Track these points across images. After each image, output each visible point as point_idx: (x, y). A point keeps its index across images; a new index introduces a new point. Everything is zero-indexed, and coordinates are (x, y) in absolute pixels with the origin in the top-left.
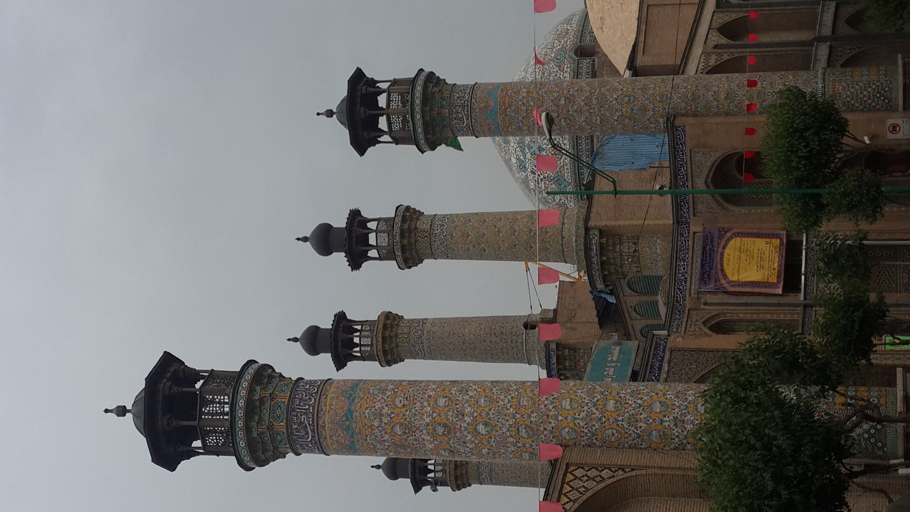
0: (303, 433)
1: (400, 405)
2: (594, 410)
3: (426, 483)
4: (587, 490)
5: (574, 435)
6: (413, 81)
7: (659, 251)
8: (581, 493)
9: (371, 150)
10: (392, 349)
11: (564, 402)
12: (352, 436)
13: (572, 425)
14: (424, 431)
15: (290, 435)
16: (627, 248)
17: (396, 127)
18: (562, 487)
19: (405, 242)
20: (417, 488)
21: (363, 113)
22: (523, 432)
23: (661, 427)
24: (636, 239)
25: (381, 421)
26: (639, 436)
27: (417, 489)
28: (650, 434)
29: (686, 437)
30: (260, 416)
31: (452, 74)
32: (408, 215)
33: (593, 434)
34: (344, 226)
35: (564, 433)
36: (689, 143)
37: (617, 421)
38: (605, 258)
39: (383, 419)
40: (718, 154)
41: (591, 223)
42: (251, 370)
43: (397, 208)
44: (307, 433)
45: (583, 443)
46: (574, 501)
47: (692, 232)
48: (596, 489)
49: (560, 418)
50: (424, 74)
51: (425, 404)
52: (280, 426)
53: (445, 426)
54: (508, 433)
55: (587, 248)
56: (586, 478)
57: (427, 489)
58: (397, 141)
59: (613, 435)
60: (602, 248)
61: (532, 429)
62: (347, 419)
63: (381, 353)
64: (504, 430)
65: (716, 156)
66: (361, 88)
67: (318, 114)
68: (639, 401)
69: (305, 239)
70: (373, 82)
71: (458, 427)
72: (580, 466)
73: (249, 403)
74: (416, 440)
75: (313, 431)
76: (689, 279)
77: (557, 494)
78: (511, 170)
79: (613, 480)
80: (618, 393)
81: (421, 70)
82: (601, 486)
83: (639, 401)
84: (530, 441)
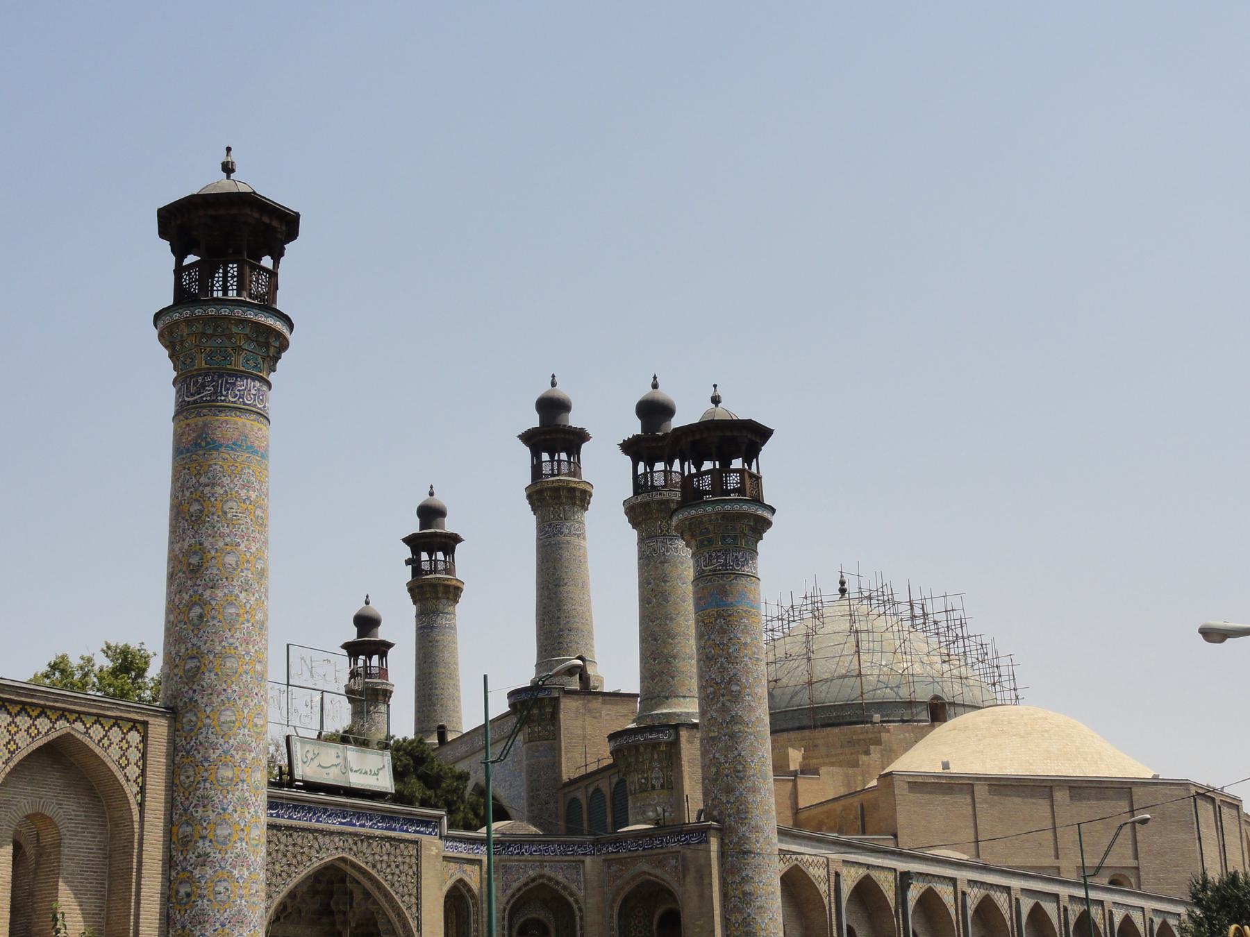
0: (192, 390)
1: (226, 508)
2: (218, 752)
3: (416, 551)
4: (106, 749)
5: (187, 728)
6: (758, 500)
8: (100, 741)
12: (188, 451)
14: (193, 541)
20: (409, 540)
22: (191, 664)
23: (196, 837)
26: (186, 810)
28: (188, 824)
29: (184, 869)
30: (212, 335)
31: (767, 545)
33: (188, 753)
34: (639, 432)
35: (190, 716)
37: (205, 781)
38: (642, 749)
39: (208, 488)
42: (279, 326)
44: (192, 395)
47: (582, 858)
50: (766, 514)
53: (200, 566)
55: (651, 729)
60: (655, 745)
61: (195, 676)
64: (194, 641)
65: (675, 887)
67: (715, 386)
68: (231, 808)
71: (198, 582)
72: (144, 739)
75: (195, 402)
76: (522, 858)
77: (95, 711)
79: (123, 781)
80: (243, 781)
81: (773, 511)
82: (114, 768)
83: (231, 808)
84: (181, 673)
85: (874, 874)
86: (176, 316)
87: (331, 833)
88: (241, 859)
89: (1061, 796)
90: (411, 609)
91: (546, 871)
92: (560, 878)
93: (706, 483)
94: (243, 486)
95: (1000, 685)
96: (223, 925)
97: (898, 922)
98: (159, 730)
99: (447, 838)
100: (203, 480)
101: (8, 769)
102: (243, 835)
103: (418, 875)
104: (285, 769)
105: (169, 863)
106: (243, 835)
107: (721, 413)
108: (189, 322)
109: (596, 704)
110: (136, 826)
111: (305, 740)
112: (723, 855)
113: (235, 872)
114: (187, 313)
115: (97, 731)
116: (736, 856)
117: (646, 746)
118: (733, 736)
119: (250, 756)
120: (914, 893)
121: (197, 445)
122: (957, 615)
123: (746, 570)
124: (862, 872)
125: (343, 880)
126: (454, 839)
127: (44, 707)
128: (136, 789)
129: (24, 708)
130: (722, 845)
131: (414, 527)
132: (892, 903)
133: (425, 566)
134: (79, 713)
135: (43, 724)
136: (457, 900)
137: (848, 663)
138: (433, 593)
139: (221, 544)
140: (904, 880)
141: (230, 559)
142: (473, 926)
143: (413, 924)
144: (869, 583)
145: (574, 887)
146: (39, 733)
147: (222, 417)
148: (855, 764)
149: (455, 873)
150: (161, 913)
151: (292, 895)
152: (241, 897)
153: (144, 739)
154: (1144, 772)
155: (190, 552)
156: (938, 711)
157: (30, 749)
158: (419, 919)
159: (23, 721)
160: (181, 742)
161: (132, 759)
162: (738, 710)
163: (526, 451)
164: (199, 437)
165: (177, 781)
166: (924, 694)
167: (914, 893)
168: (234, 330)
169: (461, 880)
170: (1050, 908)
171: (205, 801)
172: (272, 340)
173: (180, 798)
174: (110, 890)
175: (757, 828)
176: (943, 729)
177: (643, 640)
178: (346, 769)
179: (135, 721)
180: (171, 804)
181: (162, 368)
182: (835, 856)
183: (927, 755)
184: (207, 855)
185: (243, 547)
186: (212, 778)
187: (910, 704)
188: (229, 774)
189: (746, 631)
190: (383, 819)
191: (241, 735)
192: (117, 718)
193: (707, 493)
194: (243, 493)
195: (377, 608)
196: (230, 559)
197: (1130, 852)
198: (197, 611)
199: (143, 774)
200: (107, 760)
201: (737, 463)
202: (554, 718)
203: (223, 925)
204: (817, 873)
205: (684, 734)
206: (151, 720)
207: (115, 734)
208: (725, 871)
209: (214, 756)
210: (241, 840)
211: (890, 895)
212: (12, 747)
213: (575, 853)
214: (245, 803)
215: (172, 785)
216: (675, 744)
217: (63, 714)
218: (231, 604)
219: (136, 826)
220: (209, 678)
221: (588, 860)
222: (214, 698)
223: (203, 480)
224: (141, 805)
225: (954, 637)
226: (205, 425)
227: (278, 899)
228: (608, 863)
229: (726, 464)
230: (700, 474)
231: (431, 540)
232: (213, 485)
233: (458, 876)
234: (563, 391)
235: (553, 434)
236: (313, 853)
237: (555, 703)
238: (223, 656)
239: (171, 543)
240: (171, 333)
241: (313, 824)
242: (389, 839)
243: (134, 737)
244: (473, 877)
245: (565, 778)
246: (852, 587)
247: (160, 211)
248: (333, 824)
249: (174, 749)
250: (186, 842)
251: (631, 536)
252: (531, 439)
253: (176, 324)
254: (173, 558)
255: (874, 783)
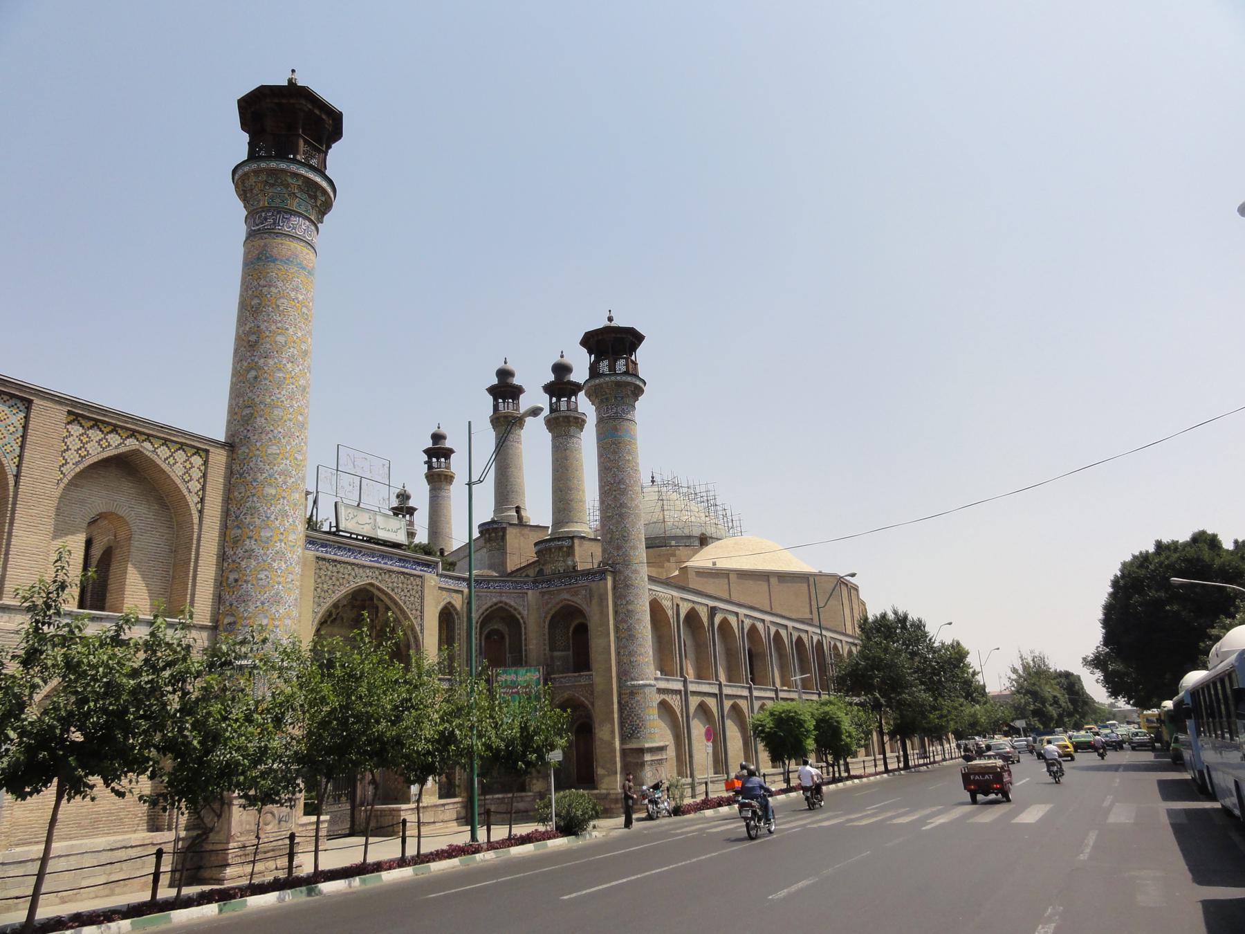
3: (430, 457)
6: (636, 376)
20: (427, 452)
22: (247, 411)
28: (238, 527)
31: (641, 403)
35: (244, 449)
36: (593, 585)
40: (585, 607)
50: (641, 384)
53: (256, 342)
55: (559, 539)
56: (188, 466)
60: (560, 548)
65: (584, 607)
72: (206, 463)
79: (185, 492)
82: (178, 481)
85: (697, 607)
86: (246, 169)
87: (364, 567)
88: (280, 555)
89: (773, 580)
90: (427, 487)
91: (504, 599)
92: (512, 603)
94: (293, 290)
95: (732, 528)
96: (263, 603)
97: (709, 635)
98: (219, 458)
99: (442, 576)
100: (262, 282)
101: (78, 470)
102: (281, 537)
103: (422, 597)
104: (334, 524)
105: (222, 557)
106: (281, 537)
107: (613, 324)
108: (257, 172)
109: (526, 531)
110: (196, 527)
111: (348, 506)
112: (615, 588)
113: (275, 565)
114: (254, 166)
115: (163, 452)
116: (623, 590)
117: (556, 545)
118: (621, 515)
119: (290, 481)
120: (717, 620)
121: (259, 259)
122: (712, 493)
123: (629, 417)
124: (690, 605)
125: (372, 599)
126: (446, 576)
127: (115, 426)
128: (196, 499)
129: (96, 424)
130: (614, 581)
131: (429, 444)
132: (706, 624)
133: (435, 465)
134: (149, 435)
135: (114, 439)
136: (447, 616)
137: (657, 516)
138: (438, 479)
139: (274, 327)
140: (713, 611)
141: (280, 339)
142: (457, 631)
143: (418, 629)
144: (667, 476)
145: (521, 609)
146: (109, 445)
147: (279, 240)
148: (662, 567)
149: (446, 598)
150: (214, 595)
151: (335, 606)
152: (279, 583)
153: (206, 463)
154: (814, 570)
155: (251, 332)
156: (704, 541)
157: (101, 457)
158: (422, 626)
159: (95, 435)
160: (236, 467)
161: (200, 486)
162: (624, 499)
163: (491, 398)
164: (261, 253)
166: (696, 532)
167: (717, 620)
168: (290, 180)
169: (449, 603)
170: (783, 633)
171: (253, 511)
172: (319, 194)
173: (233, 508)
174: (174, 577)
175: (636, 571)
176: (706, 549)
177: (554, 492)
178: (375, 527)
179: (198, 449)
180: (226, 513)
181: (238, 210)
182: (675, 594)
183: (702, 559)
184: (253, 550)
185: (291, 331)
186: (259, 494)
187: (689, 537)
188: (273, 492)
189: (629, 453)
190: (400, 560)
191: (284, 464)
192: (182, 444)
194: (293, 294)
195: (409, 490)
196: (280, 339)
197: (808, 610)
198: (253, 373)
199: (203, 488)
200: (171, 474)
202: (503, 538)
203: (263, 603)
204: (666, 604)
205: (576, 541)
206: (211, 449)
207: (180, 456)
208: (617, 597)
209: (261, 478)
210: (281, 541)
211: (705, 620)
212: (83, 453)
213: (522, 588)
214: (285, 514)
215: (227, 499)
216: (571, 547)
217: (133, 434)
218: (280, 370)
219: (196, 527)
220: (260, 421)
221: (530, 592)
222: (263, 436)
223: (262, 282)
224: (201, 512)
225: (710, 504)
226: (265, 245)
227: (325, 607)
228: (543, 594)
231: (438, 451)
232: (270, 286)
233: (448, 600)
234: (510, 366)
235: (505, 389)
236: (351, 578)
237: (504, 530)
238: (273, 406)
239: (238, 329)
240: (243, 183)
241: (352, 560)
242: (403, 573)
243: (197, 460)
244: (458, 601)
245: (509, 571)
246: (658, 479)
247: (239, 101)
248: (365, 561)
249: (230, 473)
250: (236, 541)
251: (548, 436)
252: (493, 391)
253: (246, 174)
254: (238, 338)
255: (677, 573)
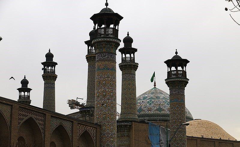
2: (110, 135)
7: (125, 143)
9: (166, 65)
10: (92, 59)
11: (112, 127)
12: (102, 69)
13: (106, 129)
15: (102, 53)
16: (126, 133)
17: (173, 72)
18: (92, 127)
19: (128, 66)
21: (177, 62)
22: (104, 116)
24: (128, 136)
25: (106, 78)
27: (42, 63)
32: (135, 66)
33: (104, 135)
37: (108, 141)
41: (133, 123)
43: (138, 64)
44: (103, 57)
45: (102, 132)
46: (89, 130)
48: (91, 136)
49: (108, 126)
51: (111, 90)
52: (104, 50)
53: (106, 95)
54: (104, 112)
57: (43, 66)
58: (168, 72)
59: (104, 140)
62: (107, 68)
63: (90, 56)
66: (184, 63)
67: (176, 50)
69: (128, 35)
70: (186, 66)
72: (96, 131)
73: (111, 42)
74: (101, 87)
78: (143, 94)
93: (102, 31)
165: (101, 140)
193: (102, 34)
201: (112, 26)
229: (108, 26)
230: (100, 28)
